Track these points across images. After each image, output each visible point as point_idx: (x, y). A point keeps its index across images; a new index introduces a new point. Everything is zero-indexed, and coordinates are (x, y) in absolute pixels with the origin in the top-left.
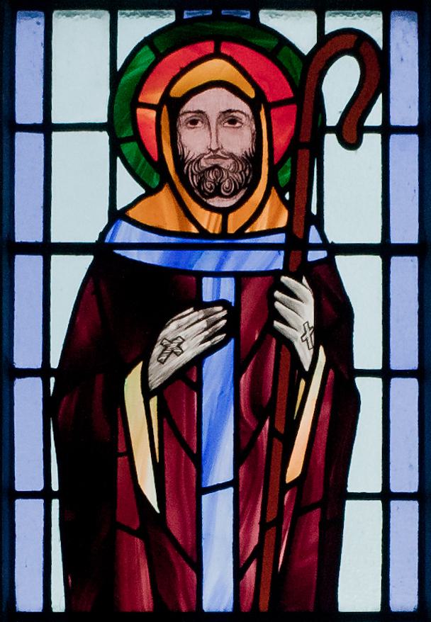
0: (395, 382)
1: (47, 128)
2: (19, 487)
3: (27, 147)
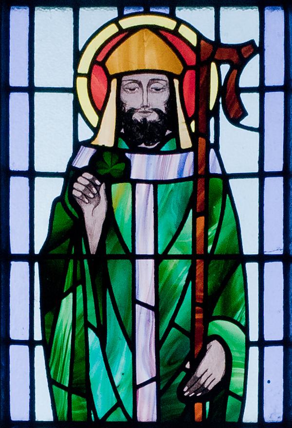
0: (267, 180)
1: (31, 90)
2: (12, 167)
3: (17, 103)
